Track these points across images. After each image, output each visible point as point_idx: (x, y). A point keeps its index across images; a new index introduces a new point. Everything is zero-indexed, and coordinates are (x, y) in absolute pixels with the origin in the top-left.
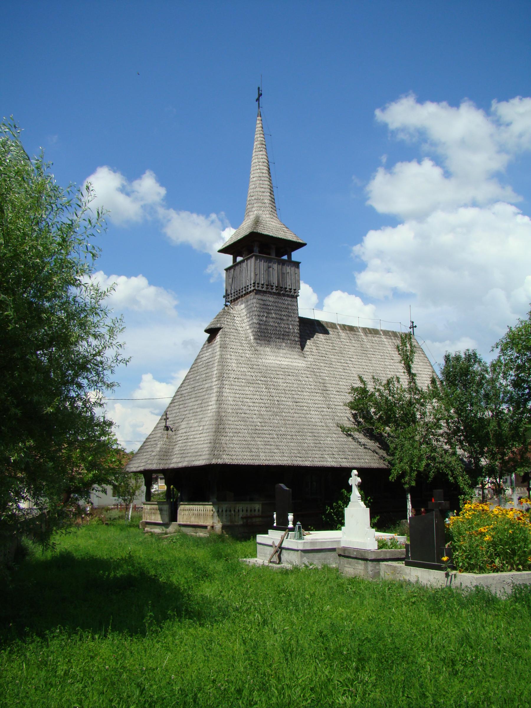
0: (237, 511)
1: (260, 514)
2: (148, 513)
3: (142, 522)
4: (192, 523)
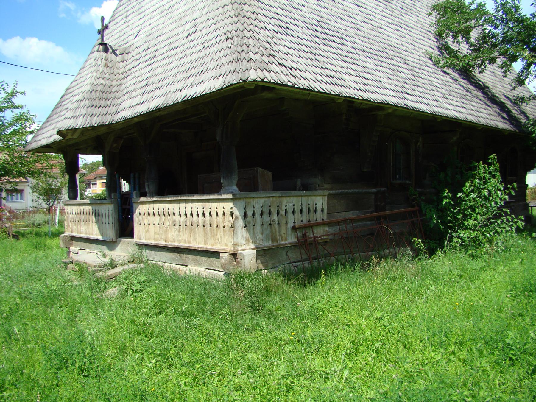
0: (283, 213)
1: (325, 218)
2: (73, 220)
3: (65, 236)
4: (170, 244)
